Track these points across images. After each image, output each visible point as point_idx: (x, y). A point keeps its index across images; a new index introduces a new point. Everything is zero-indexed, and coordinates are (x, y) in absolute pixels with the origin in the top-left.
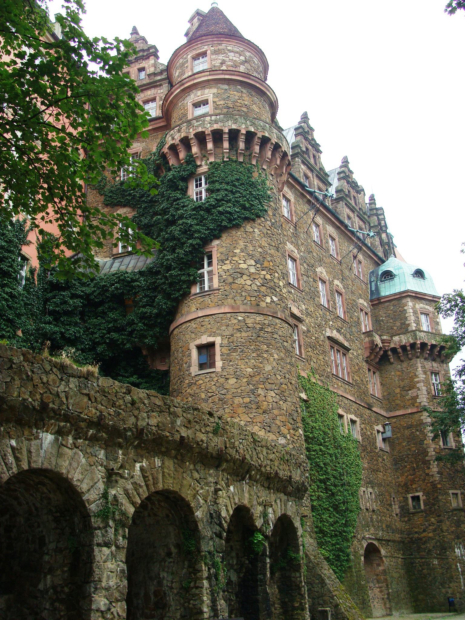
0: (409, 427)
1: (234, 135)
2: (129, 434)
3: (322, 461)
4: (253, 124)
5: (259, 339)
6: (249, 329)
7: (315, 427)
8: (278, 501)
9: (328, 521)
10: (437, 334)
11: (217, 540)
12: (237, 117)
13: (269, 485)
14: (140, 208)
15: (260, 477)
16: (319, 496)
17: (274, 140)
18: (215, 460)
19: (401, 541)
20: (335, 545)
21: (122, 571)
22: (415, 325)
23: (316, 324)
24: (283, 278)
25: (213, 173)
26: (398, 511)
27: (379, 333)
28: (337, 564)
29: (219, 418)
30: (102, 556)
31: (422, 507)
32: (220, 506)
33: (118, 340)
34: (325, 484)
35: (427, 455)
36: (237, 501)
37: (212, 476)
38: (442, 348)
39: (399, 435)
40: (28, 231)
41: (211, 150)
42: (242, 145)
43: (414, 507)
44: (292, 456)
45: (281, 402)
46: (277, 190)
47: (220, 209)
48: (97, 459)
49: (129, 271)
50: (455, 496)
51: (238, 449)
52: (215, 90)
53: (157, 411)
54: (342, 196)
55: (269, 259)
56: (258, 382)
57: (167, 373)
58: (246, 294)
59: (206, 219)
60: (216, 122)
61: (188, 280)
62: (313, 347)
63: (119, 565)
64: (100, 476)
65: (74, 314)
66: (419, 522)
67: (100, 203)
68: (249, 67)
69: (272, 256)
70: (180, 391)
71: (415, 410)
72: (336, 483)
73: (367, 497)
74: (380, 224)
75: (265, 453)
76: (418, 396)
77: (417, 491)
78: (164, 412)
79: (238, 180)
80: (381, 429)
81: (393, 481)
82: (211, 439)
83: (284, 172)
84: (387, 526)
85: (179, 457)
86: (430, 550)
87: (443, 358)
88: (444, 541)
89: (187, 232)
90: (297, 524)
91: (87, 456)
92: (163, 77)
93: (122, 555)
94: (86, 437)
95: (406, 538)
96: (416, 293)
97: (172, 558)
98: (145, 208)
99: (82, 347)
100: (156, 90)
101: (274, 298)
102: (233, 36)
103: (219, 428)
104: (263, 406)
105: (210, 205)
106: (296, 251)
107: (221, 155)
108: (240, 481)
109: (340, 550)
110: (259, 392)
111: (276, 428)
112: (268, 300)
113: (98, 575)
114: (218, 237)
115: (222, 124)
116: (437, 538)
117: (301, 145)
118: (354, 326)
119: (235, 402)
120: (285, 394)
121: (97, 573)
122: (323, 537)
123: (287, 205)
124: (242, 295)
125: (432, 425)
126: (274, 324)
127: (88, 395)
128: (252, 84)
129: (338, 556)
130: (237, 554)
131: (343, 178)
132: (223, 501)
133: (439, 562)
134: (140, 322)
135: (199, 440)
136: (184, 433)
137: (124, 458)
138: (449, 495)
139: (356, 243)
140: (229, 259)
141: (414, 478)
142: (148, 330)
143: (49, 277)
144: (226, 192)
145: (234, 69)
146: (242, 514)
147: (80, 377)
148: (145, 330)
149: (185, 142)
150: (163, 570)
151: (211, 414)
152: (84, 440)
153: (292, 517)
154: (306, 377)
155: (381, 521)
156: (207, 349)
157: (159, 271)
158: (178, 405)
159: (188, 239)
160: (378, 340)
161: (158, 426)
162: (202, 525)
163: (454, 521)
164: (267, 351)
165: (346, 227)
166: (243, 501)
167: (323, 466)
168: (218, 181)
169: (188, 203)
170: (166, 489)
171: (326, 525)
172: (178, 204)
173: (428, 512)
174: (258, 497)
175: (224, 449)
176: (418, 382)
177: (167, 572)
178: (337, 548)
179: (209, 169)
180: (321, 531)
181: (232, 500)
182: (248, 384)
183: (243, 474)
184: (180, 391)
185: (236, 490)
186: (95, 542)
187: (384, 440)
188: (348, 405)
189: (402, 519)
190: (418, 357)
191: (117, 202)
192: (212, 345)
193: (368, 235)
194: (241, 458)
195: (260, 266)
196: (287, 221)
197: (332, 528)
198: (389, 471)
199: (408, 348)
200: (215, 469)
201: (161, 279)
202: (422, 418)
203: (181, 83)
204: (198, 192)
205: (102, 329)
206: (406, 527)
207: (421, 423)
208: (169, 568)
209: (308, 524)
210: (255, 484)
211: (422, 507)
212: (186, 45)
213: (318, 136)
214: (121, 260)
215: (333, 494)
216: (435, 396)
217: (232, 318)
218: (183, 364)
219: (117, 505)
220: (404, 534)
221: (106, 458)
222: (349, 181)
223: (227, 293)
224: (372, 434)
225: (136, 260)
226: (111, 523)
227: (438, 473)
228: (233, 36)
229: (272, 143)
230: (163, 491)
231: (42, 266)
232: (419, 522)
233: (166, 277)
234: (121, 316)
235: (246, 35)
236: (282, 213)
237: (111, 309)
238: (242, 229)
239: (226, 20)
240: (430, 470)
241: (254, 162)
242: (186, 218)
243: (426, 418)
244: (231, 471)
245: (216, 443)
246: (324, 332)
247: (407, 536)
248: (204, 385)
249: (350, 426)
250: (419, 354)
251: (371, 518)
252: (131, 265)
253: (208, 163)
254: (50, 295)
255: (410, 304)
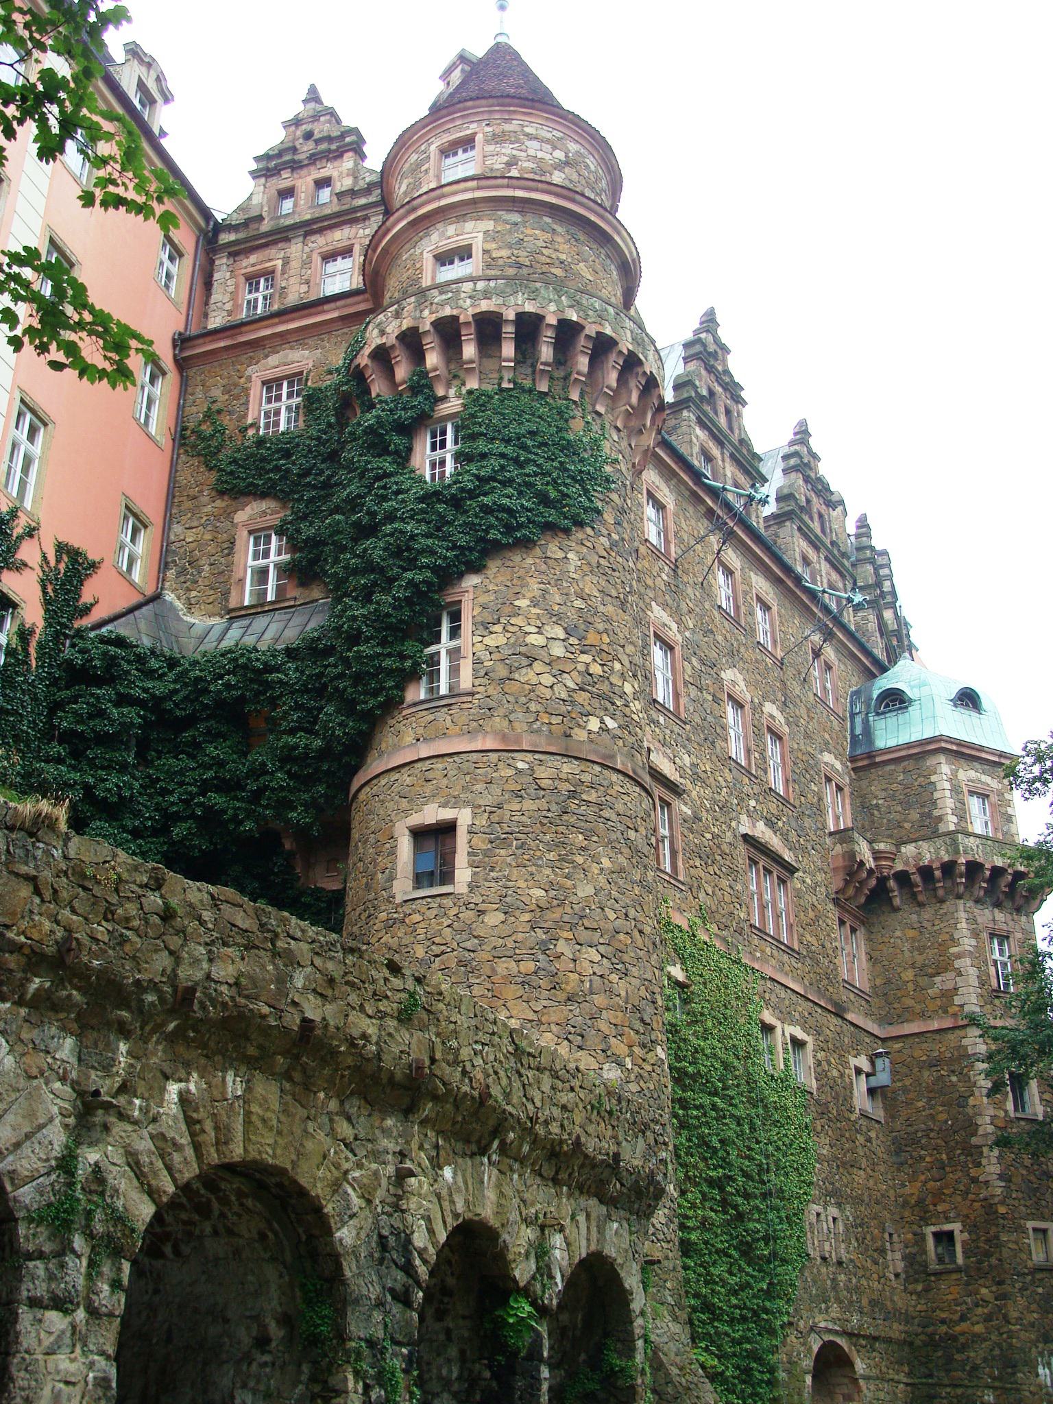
0: (933, 1064)
1: (528, 327)
2: (150, 998)
3: (718, 1135)
4: (576, 304)
5: (565, 817)
6: (542, 793)
7: (703, 1050)
8: (581, 1218)
9: (724, 1283)
10: (1005, 842)
11: (394, 1311)
12: (538, 285)
13: (557, 1173)
14: (298, 500)
15: (531, 1150)
16: (705, 1219)
17: (626, 345)
18: (400, 1090)
19: (905, 1341)
20: (740, 1343)
21: (102, 1382)
22: (955, 819)
23: (715, 802)
24: (635, 676)
25: (473, 416)
26: (900, 1266)
27: (869, 835)
28: (743, 1391)
29: (419, 980)
30: (43, 1334)
31: (960, 1260)
32: (410, 1219)
33: (224, 811)
34: (722, 1189)
35: (974, 1134)
36: (460, 1207)
37: (390, 1134)
38: (1019, 876)
39: (908, 1082)
40: (20, 538)
41: (472, 362)
42: (546, 352)
43: (940, 1260)
44: (624, 1104)
45: (614, 977)
46: (630, 466)
47: (486, 500)
48: (50, 1060)
49: (263, 646)
50: (1040, 1236)
51: (469, 1068)
52: (488, 225)
53: (238, 945)
54: (791, 510)
55: (601, 627)
56: (559, 925)
57: (338, 899)
58: (539, 708)
59: (449, 523)
60: (487, 295)
61: (397, 669)
62: (707, 858)
63: (92, 1364)
64: (55, 1110)
65: (122, 742)
66: (950, 1297)
67: (206, 487)
68: (575, 177)
69: (609, 620)
70: (366, 938)
71: (948, 1023)
72: (750, 1190)
73: (824, 1228)
74: (879, 584)
75: (546, 1087)
76: (956, 989)
77: (948, 1220)
78: (258, 948)
79: (532, 434)
80: (865, 1065)
81: (892, 1193)
82: (390, 1035)
83: (648, 424)
84: (873, 1303)
85: (297, 1076)
86: (975, 1368)
87: (1019, 901)
88: (1011, 1345)
89: (403, 552)
90: (631, 1280)
91: (19, 1048)
92: (372, 199)
93: (107, 1337)
94: (21, 997)
95: (917, 1335)
96: (960, 743)
97: (270, 1352)
98: (311, 500)
99: (137, 823)
100: (354, 230)
101: (607, 720)
102: (539, 101)
103: (416, 1005)
104: (567, 983)
105: (462, 490)
106: (674, 626)
107: (496, 375)
108: (472, 1155)
109: (754, 1356)
110: (559, 949)
111: (597, 1040)
112: (594, 724)
113: (23, 1389)
114: (477, 568)
115: (500, 301)
116: (993, 1337)
117: (697, 383)
118: (809, 816)
119: (499, 970)
120: (626, 958)
121: (20, 1383)
122: (712, 1321)
123: (655, 516)
124: (528, 710)
125: (990, 1057)
126: (605, 783)
127: (32, 880)
128: (582, 213)
129: (747, 1371)
130: (462, 1352)
131: (795, 469)
132: (420, 1206)
133: (997, 1397)
134: (281, 768)
135: (356, 1033)
136: (313, 1009)
137: (131, 1065)
138: (1025, 1231)
139: (819, 620)
140: (503, 620)
141: (941, 1188)
142: (299, 791)
143: (67, 652)
144: (502, 461)
145: (537, 177)
146: (473, 1244)
147: (11, 828)
148: (291, 790)
149: (412, 341)
150: (244, 1386)
151: (394, 968)
152: (14, 1003)
153: (619, 1261)
154: (685, 926)
155: (857, 1289)
156: (437, 836)
157: (333, 647)
158: (299, 934)
159: (405, 570)
160: (864, 851)
161: (237, 984)
162: (354, 1266)
163: (1037, 1297)
164: (584, 849)
165: (798, 579)
166: (478, 1211)
167: (718, 1145)
168: (485, 435)
169: (408, 484)
170: (255, 1162)
171: (718, 1293)
172: (384, 487)
173: (974, 1274)
174: (524, 1202)
175: (427, 1063)
176: (959, 956)
177: (255, 1392)
178: (746, 1350)
179: (464, 405)
180: (707, 1307)
181: (446, 1204)
182: (533, 928)
183: (481, 1138)
184: (366, 938)
185: (460, 1179)
186: (25, 1293)
187: (872, 1092)
188: (787, 1003)
189: (910, 1287)
190: (959, 897)
191: (247, 487)
192: (447, 829)
193: (850, 600)
194: (476, 1093)
195: (577, 642)
196: (656, 553)
197: (734, 1301)
198: (882, 1168)
199: (938, 873)
200: (401, 1117)
201: (335, 666)
202: (965, 1042)
203: (410, 205)
204: (433, 461)
205: (188, 784)
206: (919, 1307)
207: (963, 1057)
208: (258, 1381)
209: (669, 1285)
210: (516, 1166)
211: (960, 1260)
212: (427, 121)
213: (737, 366)
214: (245, 622)
215: (740, 1217)
216: (999, 991)
217: (501, 765)
218: (376, 873)
219: (102, 1194)
220: (912, 1324)
221: (80, 1060)
222: (809, 476)
223: (492, 704)
224: (842, 1075)
225: (282, 624)
226: (78, 1242)
227: (1001, 1177)
228: (539, 101)
229: (620, 352)
230: (244, 1163)
231: (50, 625)
232: (950, 1297)
233: (346, 662)
234: (234, 752)
235: (568, 101)
236: (643, 533)
237: (213, 736)
238: (538, 551)
239: (526, 72)
240: (980, 1170)
241: (575, 396)
242: (403, 520)
243: (976, 1044)
244: (448, 1126)
245: (405, 1046)
246: (733, 824)
247: (920, 1330)
248: (423, 925)
249: (790, 1052)
250: (962, 889)
251: (834, 1280)
252: (269, 635)
253: (464, 392)
254: (64, 694)
255: (945, 769)
